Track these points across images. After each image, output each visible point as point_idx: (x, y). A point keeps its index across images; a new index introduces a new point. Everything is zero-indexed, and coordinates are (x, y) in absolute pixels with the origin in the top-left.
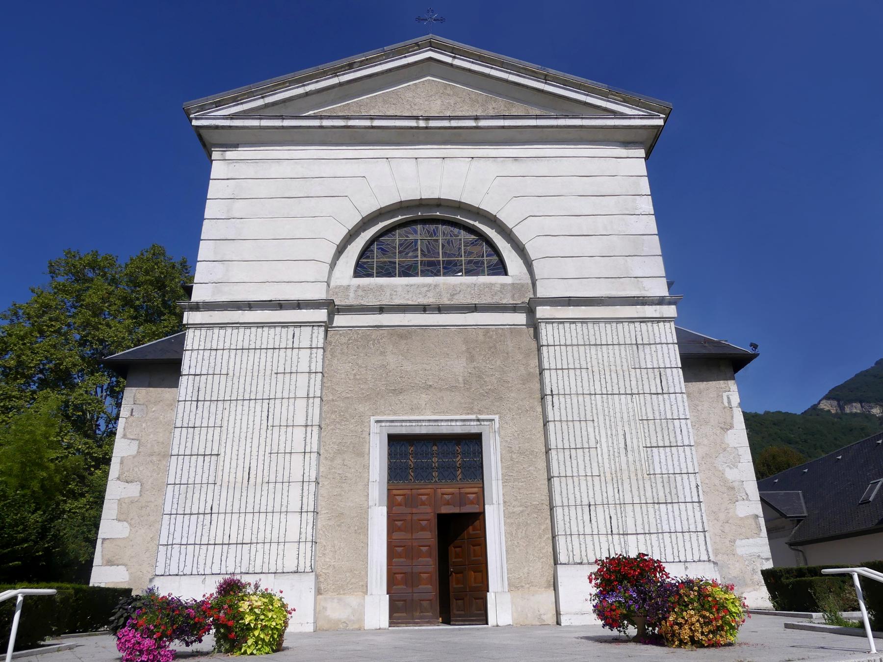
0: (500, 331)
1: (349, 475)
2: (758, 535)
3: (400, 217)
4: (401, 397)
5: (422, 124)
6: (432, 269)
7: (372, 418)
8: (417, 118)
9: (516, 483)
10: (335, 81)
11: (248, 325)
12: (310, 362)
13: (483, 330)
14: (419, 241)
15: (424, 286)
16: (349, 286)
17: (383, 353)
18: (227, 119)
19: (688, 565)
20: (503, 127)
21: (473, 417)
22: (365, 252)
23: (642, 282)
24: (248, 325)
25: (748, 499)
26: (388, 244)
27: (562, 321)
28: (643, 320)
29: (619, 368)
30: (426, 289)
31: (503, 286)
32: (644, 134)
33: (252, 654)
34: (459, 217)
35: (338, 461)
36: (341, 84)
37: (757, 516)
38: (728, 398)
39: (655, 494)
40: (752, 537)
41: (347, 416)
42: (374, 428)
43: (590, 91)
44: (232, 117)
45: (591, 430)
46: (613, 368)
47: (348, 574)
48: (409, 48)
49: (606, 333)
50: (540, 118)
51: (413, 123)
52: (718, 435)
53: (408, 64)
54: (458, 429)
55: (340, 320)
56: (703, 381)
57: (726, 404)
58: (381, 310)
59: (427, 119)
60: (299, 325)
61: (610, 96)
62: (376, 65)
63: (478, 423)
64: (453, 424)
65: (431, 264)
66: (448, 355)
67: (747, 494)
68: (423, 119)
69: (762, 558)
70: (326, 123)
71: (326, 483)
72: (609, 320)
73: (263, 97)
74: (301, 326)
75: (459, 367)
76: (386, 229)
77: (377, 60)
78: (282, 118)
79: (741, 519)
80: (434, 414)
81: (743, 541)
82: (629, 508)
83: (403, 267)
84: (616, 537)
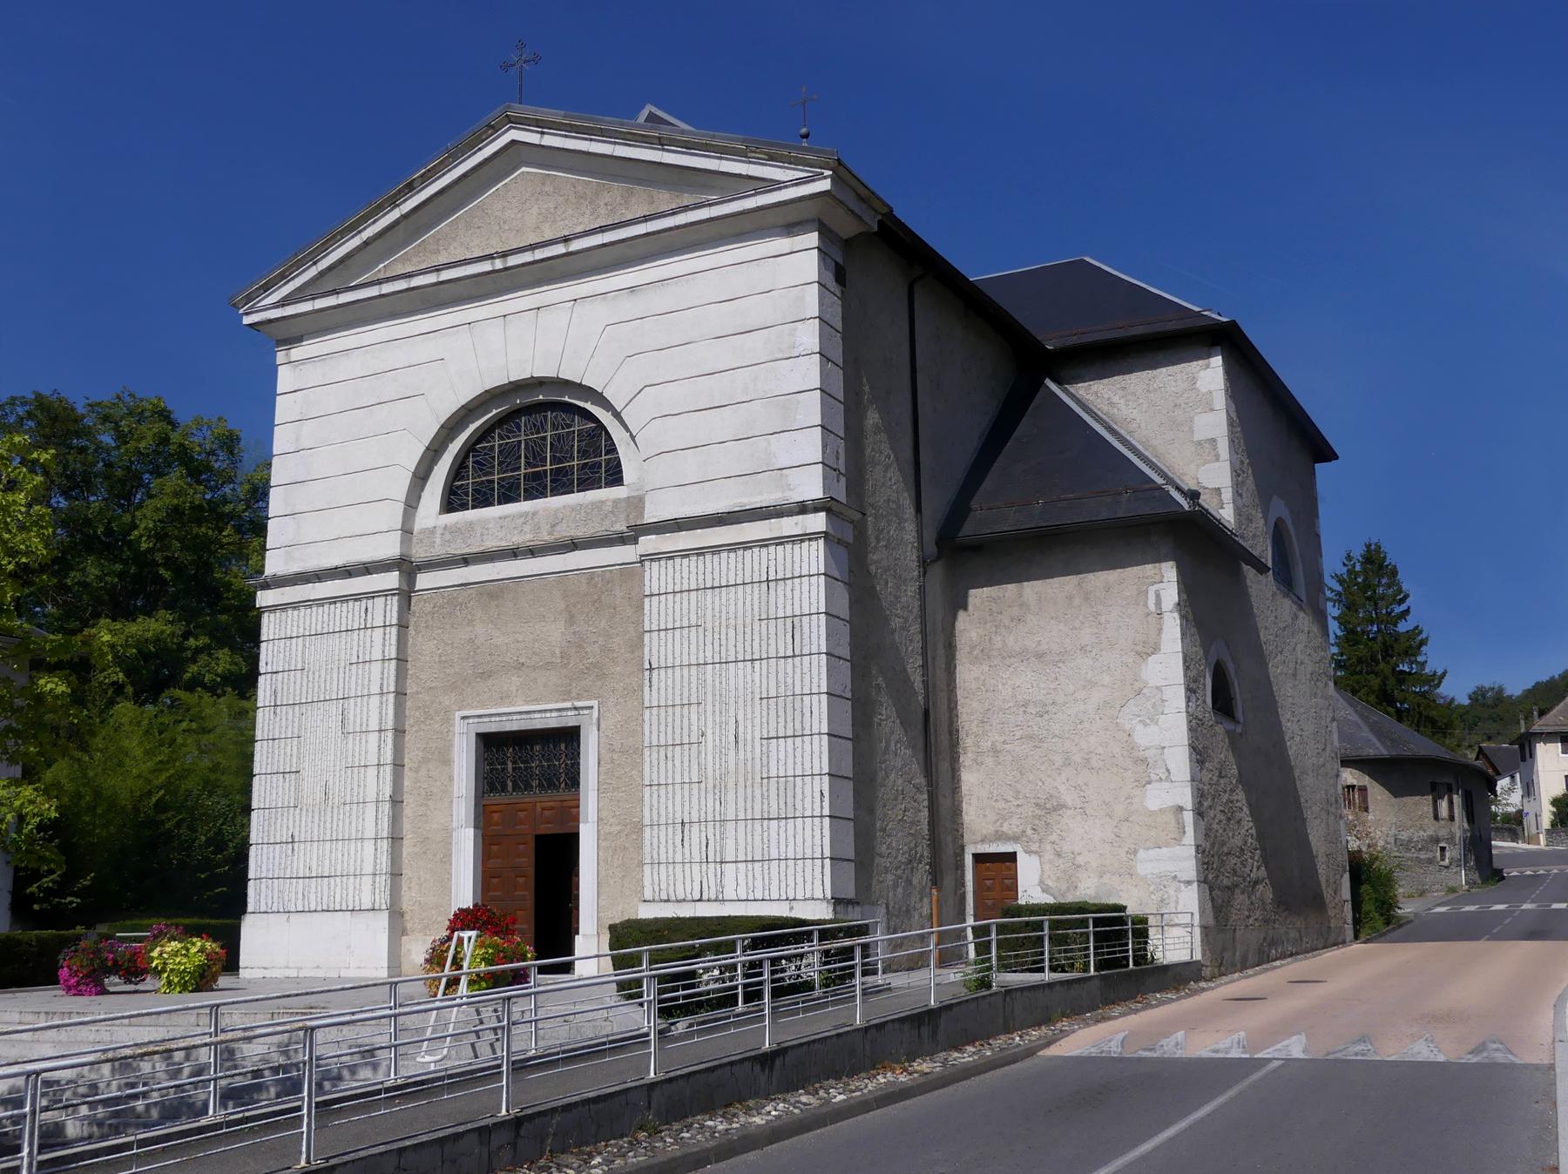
0: (608, 575)
1: (435, 790)
2: (1178, 841)
3: (494, 412)
4: (490, 683)
5: (499, 264)
6: (536, 488)
7: (457, 713)
8: (490, 257)
9: (615, 793)
10: (395, 215)
11: (320, 602)
12: (384, 645)
13: (587, 576)
14: (523, 442)
15: (521, 515)
16: (435, 527)
17: (470, 623)
18: (277, 307)
19: (794, 904)
20: (604, 245)
21: (568, 705)
22: (458, 471)
23: (786, 476)
24: (320, 602)
25: (1169, 779)
26: (486, 454)
27: (670, 556)
28: (780, 541)
29: (740, 622)
30: (522, 520)
31: (616, 502)
32: (812, 210)
33: (165, 993)
34: (567, 399)
35: (423, 772)
36: (405, 217)
37: (1181, 809)
38: (1158, 596)
39: (765, 806)
40: (1167, 845)
41: (432, 712)
42: (459, 726)
43: (723, 152)
44: (283, 303)
45: (694, 717)
46: (732, 622)
47: (434, 912)
48: (481, 135)
49: (727, 567)
50: (651, 220)
51: (486, 267)
52: (1130, 665)
53: (486, 159)
54: (552, 721)
55: (424, 581)
56: (1114, 568)
57: (1152, 607)
58: (466, 561)
59: (504, 255)
60: (372, 595)
61: (749, 155)
62: (444, 174)
63: (577, 712)
64: (548, 715)
65: (537, 476)
66: (544, 616)
67: (1168, 770)
68: (499, 257)
69: (1179, 881)
70: (387, 288)
71: (411, 801)
72: (733, 547)
73: (315, 263)
74: (373, 597)
75: (555, 633)
76: (481, 432)
77: (442, 167)
78: (335, 292)
79: (1153, 812)
80: (527, 702)
81: (1151, 852)
82: (730, 826)
83: (503, 486)
84: (712, 866)
